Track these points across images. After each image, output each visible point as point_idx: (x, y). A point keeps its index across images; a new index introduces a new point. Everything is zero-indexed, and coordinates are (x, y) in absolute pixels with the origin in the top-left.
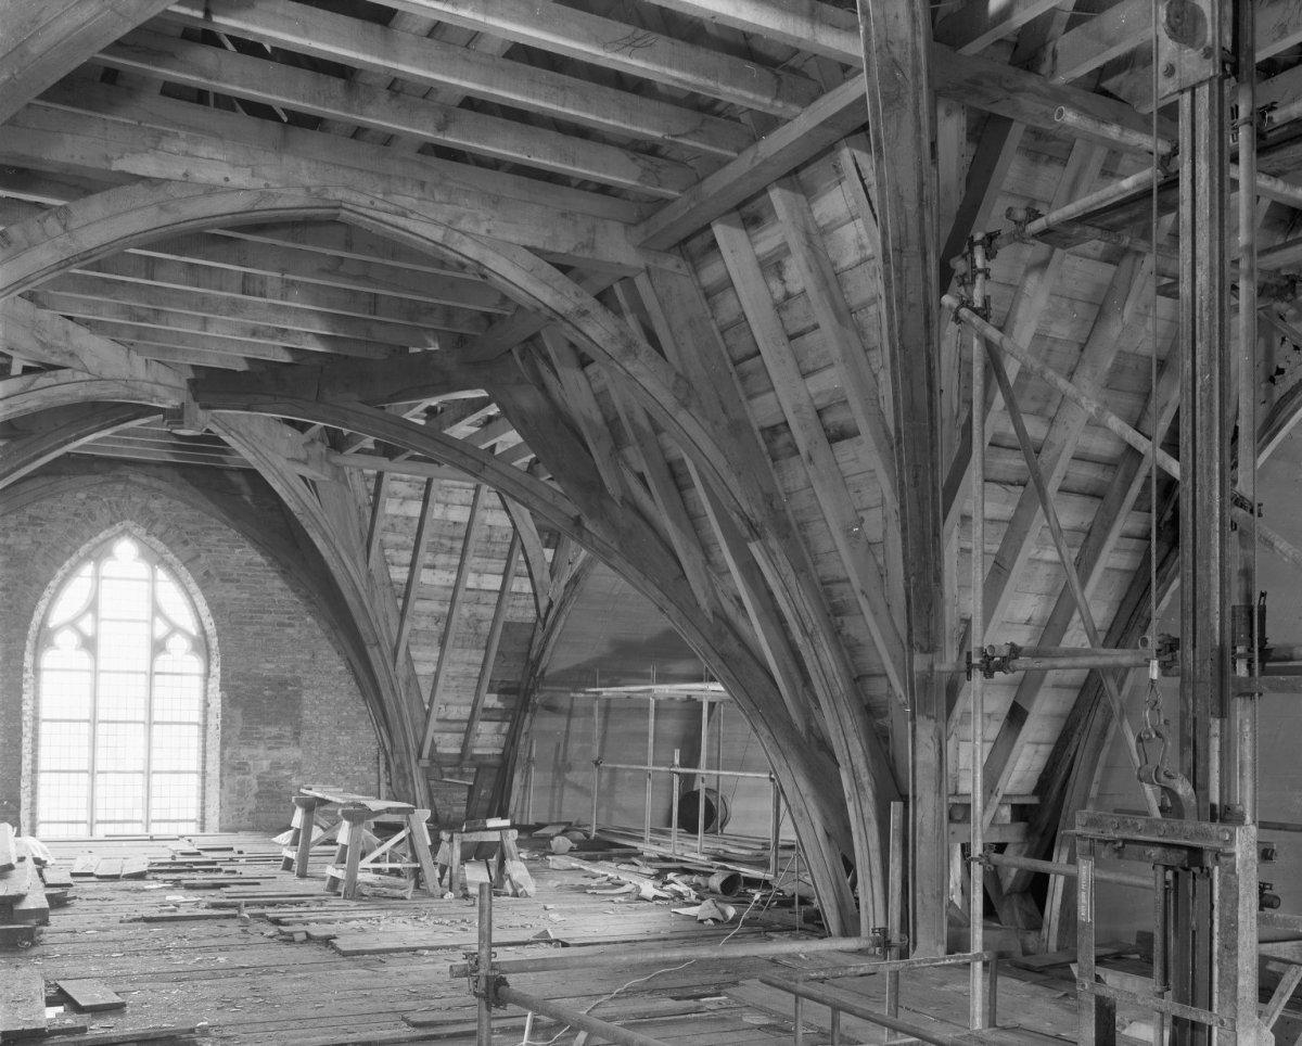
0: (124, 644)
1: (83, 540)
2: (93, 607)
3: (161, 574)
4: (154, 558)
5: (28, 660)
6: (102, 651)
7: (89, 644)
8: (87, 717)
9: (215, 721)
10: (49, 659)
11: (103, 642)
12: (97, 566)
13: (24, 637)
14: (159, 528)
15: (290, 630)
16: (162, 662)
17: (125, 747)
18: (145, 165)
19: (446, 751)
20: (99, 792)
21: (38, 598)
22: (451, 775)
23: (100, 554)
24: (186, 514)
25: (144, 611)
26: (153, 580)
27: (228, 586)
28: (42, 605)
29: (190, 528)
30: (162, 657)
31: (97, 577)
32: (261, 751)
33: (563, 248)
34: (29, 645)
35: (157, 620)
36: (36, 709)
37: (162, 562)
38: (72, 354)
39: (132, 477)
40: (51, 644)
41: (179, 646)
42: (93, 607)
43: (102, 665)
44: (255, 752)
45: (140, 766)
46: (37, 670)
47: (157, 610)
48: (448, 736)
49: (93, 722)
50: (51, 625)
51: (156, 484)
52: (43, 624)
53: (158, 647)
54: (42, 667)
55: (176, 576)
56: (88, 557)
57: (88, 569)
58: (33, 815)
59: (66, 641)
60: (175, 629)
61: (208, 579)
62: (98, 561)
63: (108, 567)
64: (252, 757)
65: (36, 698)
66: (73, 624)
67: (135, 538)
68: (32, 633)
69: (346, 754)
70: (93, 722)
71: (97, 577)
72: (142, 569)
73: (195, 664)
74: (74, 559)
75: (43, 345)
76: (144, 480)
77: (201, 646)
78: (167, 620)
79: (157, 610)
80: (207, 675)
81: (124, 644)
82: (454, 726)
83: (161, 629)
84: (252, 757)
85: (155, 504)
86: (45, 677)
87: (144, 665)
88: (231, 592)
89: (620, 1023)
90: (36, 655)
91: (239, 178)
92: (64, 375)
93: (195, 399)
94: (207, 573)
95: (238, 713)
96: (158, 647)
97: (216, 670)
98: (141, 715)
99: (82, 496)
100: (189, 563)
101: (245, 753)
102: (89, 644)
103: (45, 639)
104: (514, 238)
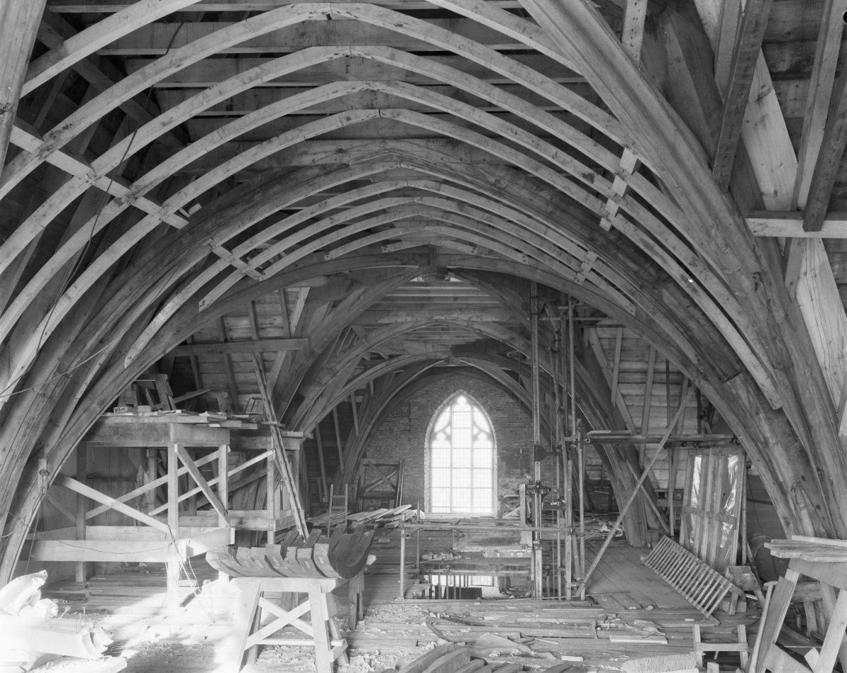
0: (462, 437)
1: (444, 399)
2: (450, 423)
3: (475, 409)
4: (472, 403)
5: (426, 445)
6: (455, 440)
7: (449, 438)
8: (449, 466)
9: (496, 467)
10: (435, 444)
11: (454, 436)
12: (451, 408)
13: (424, 437)
14: (472, 391)
15: (525, 429)
16: (477, 444)
17: (463, 478)
18: (386, 321)
19: (593, 479)
20: (454, 495)
21: (429, 421)
22: (597, 490)
23: (452, 402)
24: (482, 385)
25: (469, 424)
26: (472, 411)
27: (499, 412)
28: (431, 424)
29: (484, 390)
30: (476, 442)
31: (451, 412)
32: (514, 479)
33: (505, 320)
34: (426, 440)
35: (474, 427)
36: (430, 463)
37: (475, 404)
38: (404, 350)
39: (461, 373)
40: (435, 438)
41: (483, 437)
42: (450, 423)
43: (454, 446)
44: (511, 480)
45: (469, 485)
46: (430, 449)
47: (474, 424)
48: (593, 472)
49: (451, 468)
50: (435, 431)
51: (470, 374)
52: (433, 429)
53: (475, 438)
54: (195, 431)
55: (480, 409)
56: (448, 404)
57: (448, 409)
58: (430, 504)
59: (441, 437)
60: (481, 430)
61: (492, 410)
62: (451, 405)
63: (456, 408)
64: (511, 482)
65: (430, 459)
66: (443, 431)
67: (465, 396)
68: (427, 435)
69: (549, 480)
70: (451, 468)
71: (451, 412)
72: (468, 407)
73: (489, 444)
74: (441, 406)
75: (393, 350)
76: (465, 373)
77: (491, 437)
78: (478, 427)
79: (474, 424)
80: (494, 448)
81: (462, 437)
82: (596, 468)
83: (476, 431)
84: (511, 482)
85: (471, 382)
86: (434, 451)
87: (469, 446)
88: (500, 415)
89: (363, 476)
90: (430, 443)
91: (409, 319)
92: (401, 358)
93: (453, 354)
94: (491, 408)
95: (504, 464)
96: (475, 438)
97: (496, 446)
98: (469, 465)
99: (443, 381)
100: (484, 404)
101: (507, 480)
102: (449, 438)
103: (433, 436)
104: (490, 320)
